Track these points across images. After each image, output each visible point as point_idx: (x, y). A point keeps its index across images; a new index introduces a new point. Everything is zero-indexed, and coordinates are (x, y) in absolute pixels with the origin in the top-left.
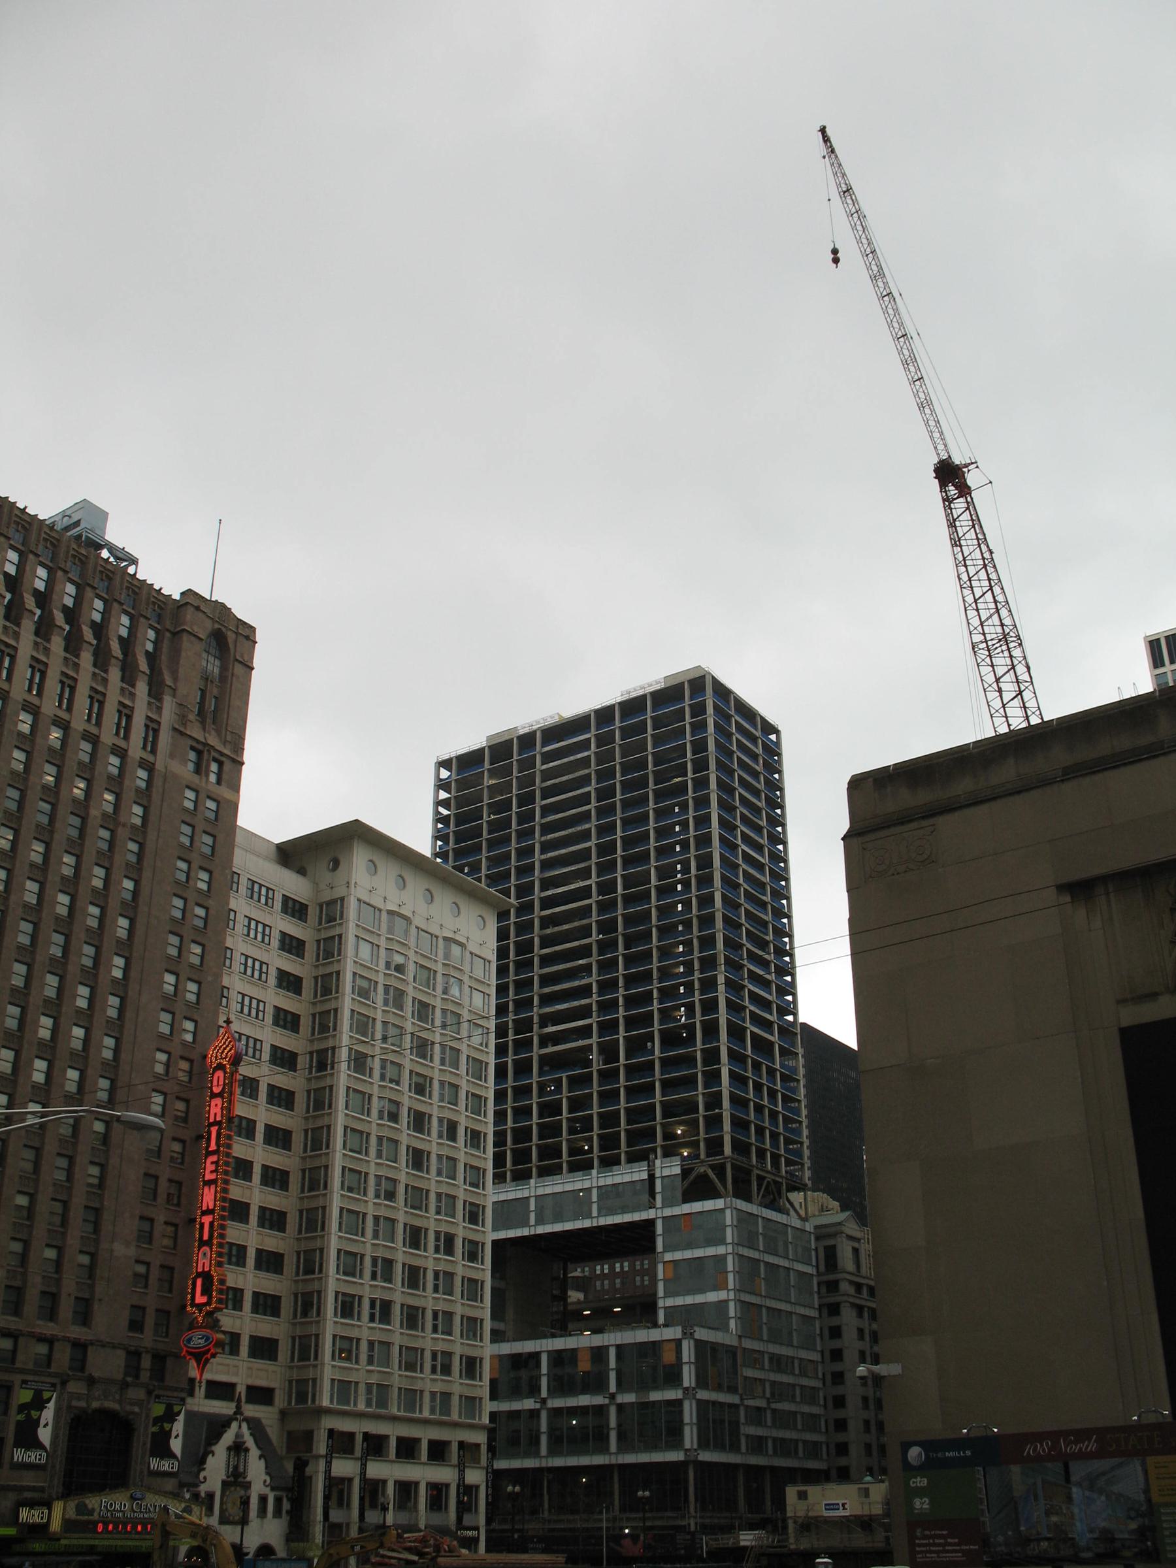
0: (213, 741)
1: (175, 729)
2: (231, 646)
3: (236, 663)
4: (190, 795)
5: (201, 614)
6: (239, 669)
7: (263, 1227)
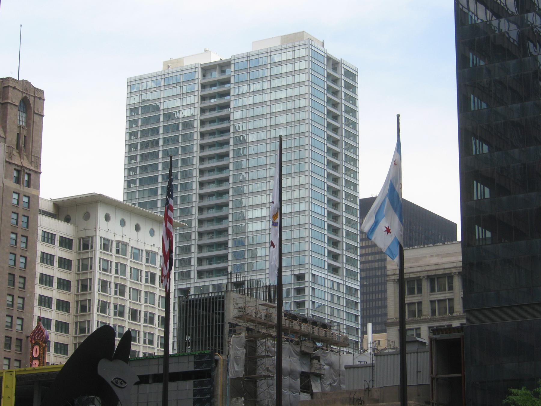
0: (26, 164)
1: (6, 162)
2: (32, 106)
3: (35, 115)
4: (15, 196)
5: (16, 91)
6: (36, 118)
7: (57, 353)
